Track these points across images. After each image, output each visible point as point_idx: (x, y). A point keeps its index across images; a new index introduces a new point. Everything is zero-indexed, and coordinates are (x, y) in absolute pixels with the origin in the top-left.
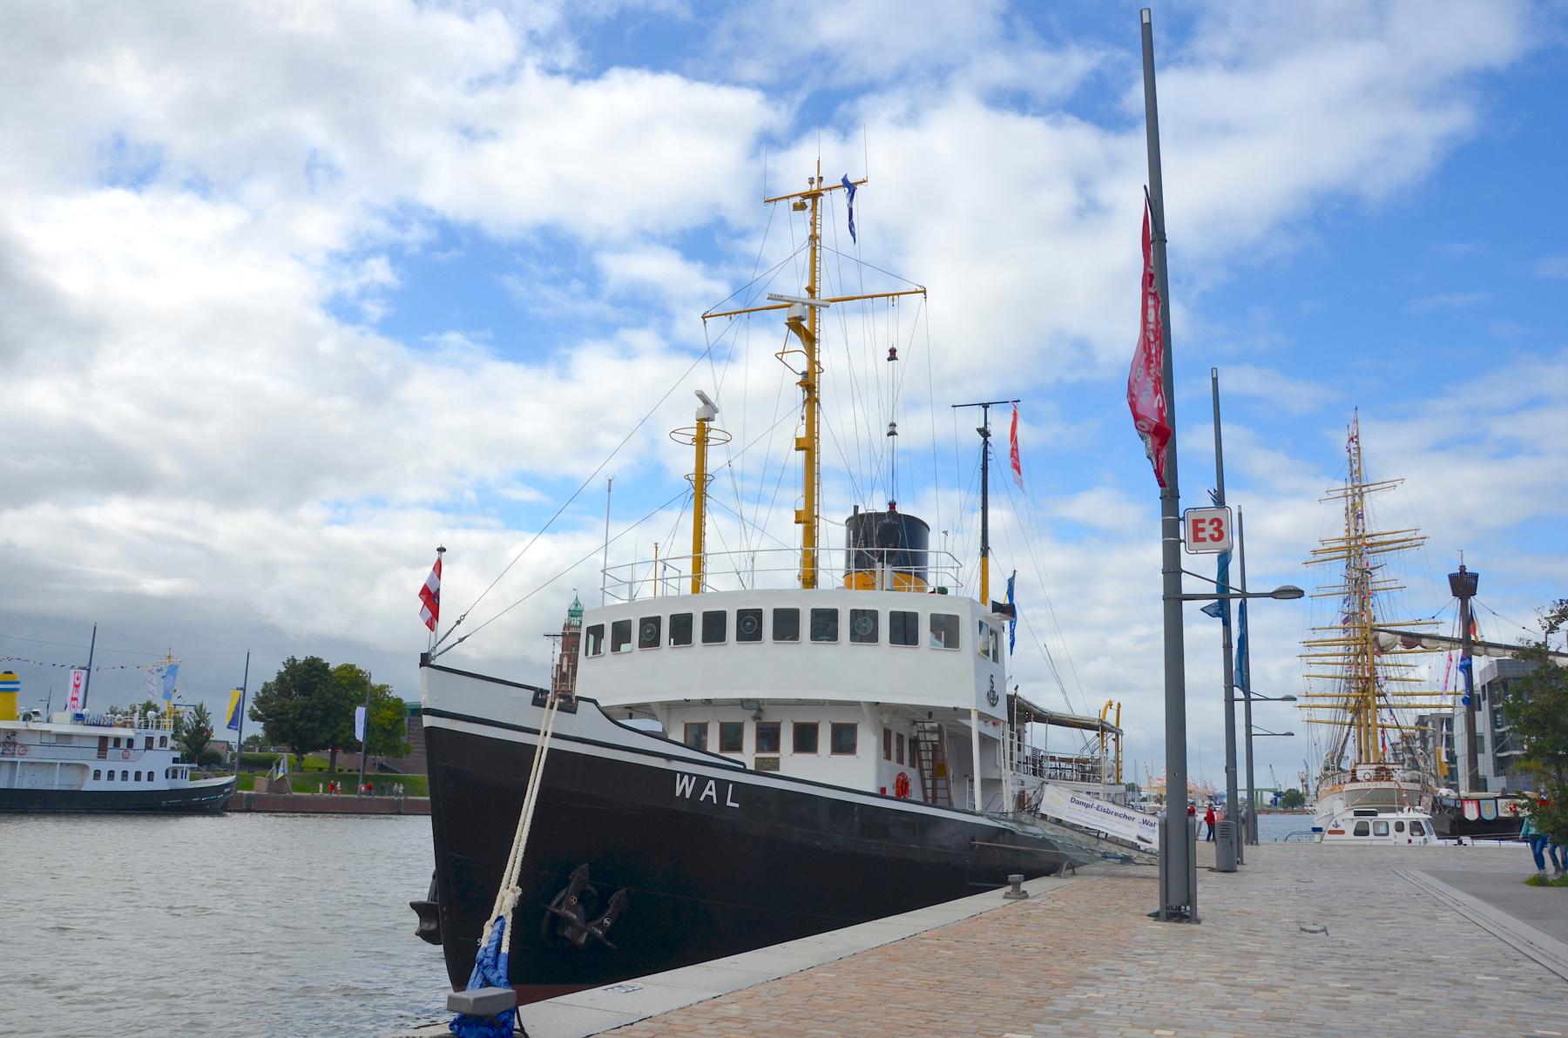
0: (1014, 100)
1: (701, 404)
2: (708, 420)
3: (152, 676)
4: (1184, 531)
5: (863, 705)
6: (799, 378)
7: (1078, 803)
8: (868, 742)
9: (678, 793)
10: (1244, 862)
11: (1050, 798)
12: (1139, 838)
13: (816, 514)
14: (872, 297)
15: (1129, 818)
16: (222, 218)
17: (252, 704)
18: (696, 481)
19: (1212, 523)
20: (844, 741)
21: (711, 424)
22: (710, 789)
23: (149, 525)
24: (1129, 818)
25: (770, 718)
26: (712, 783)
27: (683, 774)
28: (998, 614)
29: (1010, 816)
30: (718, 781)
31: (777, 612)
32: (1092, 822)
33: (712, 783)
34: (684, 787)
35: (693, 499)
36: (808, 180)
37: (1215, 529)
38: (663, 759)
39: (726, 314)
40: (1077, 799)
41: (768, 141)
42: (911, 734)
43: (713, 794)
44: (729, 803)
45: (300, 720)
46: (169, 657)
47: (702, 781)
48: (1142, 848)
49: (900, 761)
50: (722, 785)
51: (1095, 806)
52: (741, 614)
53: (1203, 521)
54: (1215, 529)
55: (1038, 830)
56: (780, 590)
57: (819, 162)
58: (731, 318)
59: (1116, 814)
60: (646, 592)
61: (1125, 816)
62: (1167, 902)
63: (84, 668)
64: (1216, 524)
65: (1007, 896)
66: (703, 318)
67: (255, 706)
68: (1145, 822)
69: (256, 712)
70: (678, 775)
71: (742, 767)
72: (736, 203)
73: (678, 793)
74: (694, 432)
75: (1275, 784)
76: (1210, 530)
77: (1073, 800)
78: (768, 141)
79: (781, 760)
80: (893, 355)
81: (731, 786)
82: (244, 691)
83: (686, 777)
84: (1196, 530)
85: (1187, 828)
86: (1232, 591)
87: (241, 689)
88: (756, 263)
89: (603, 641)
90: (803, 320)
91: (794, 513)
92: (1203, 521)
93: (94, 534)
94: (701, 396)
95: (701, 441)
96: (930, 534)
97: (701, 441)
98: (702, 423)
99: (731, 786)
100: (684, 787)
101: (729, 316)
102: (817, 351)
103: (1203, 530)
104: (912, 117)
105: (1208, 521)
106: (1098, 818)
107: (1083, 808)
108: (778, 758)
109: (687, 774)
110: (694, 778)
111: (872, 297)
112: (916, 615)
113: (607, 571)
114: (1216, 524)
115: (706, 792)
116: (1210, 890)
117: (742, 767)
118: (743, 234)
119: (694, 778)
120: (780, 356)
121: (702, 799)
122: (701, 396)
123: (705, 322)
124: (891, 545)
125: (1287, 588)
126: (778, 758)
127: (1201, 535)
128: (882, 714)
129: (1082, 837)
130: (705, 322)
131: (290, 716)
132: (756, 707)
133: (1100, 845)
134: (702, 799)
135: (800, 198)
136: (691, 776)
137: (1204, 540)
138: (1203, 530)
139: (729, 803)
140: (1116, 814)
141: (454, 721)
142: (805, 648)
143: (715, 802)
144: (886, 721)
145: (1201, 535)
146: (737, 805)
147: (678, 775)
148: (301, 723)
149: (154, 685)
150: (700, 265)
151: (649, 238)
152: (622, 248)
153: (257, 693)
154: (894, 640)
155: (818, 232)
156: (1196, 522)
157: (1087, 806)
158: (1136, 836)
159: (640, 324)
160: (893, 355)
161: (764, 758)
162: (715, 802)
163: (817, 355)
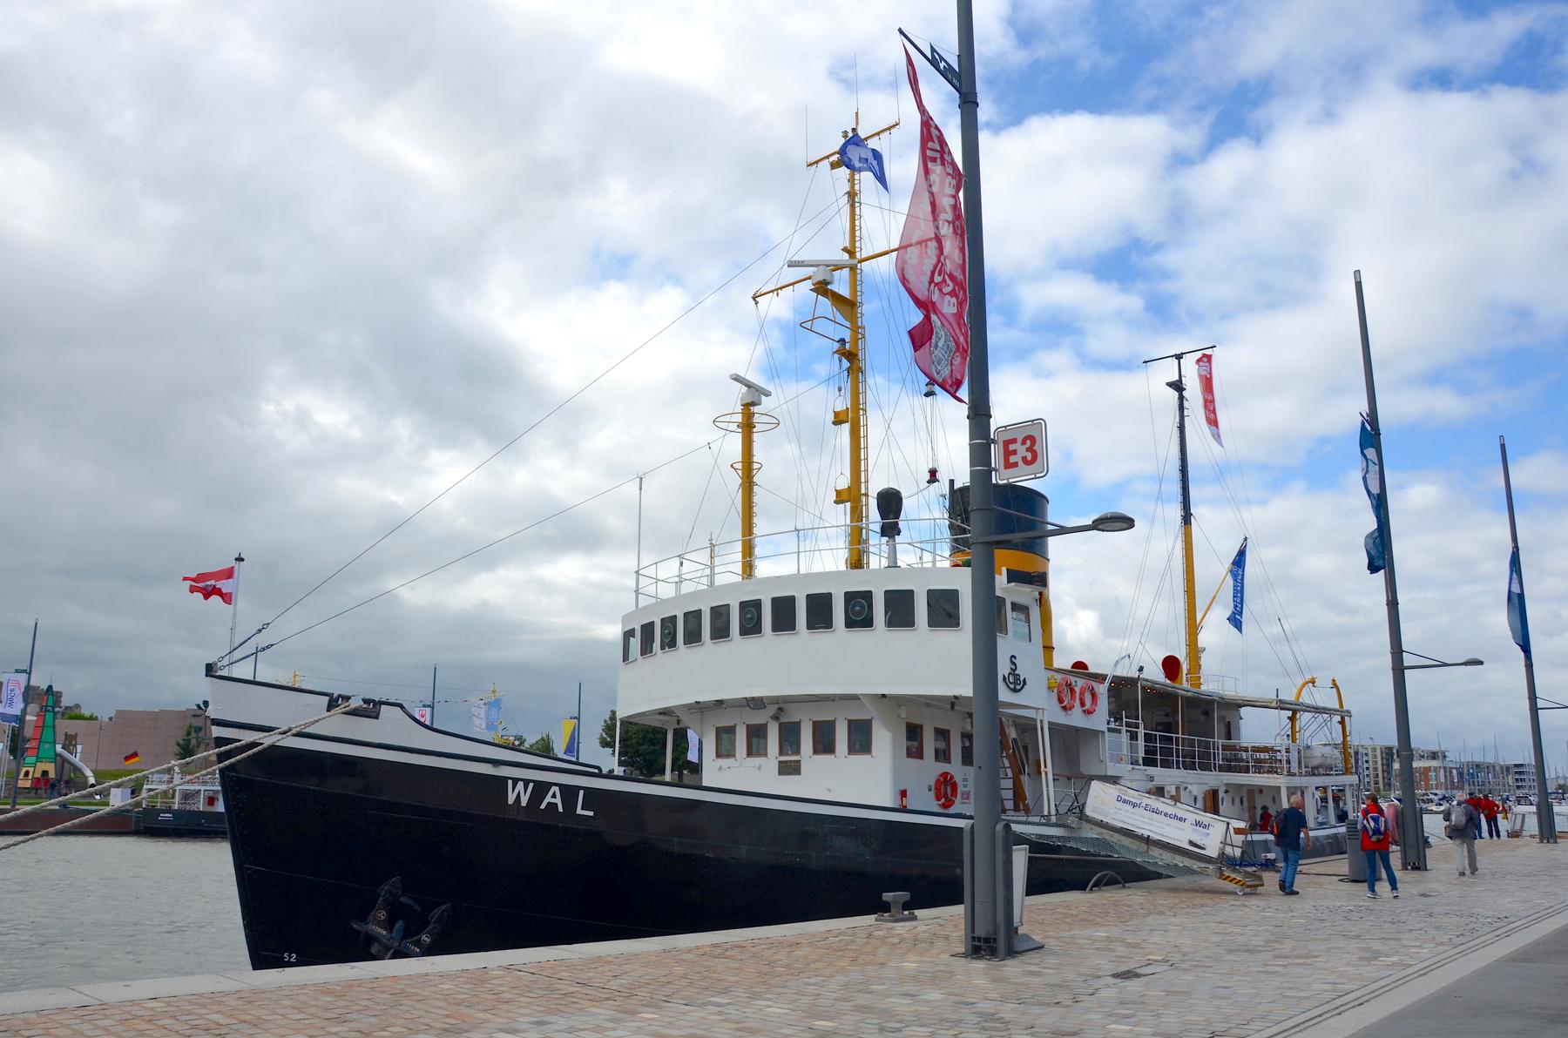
0: (1440, 79)
1: (745, 389)
2: (753, 404)
3: (479, 710)
4: (996, 452)
5: (863, 699)
6: (837, 346)
7: (1125, 801)
8: (884, 740)
10: (1428, 868)
11: (1095, 797)
12: (1192, 843)
13: (863, 491)
15: (1180, 819)
16: (671, 299)
17: (601, 731)
18: (743, 469)
19: (1024, 442)
20: (861, 741)
21: (755, 409)
22: (554, 796)
23: (595, 576)
24: (1180, 819)
25: (792, 716)
27: (516, 781)
28: (1013, 584)
29: (1053, 819)
30: (563, 787)
31: (775, 601)
32: (1138, 823)
34: (518, 795)
35: (741, 490)
36: (842, 134)
37: (1028, 450)
38: (490, 765)
39: (772, 291)
40: (1123, 797)
41: (1180, 161)
42: (964, 728)
43: (558, 801)
44: (579, 811)
45: (643, 744)
46: (494, 692)
47: (541, 788)
49: (943, 755)
50: (569, 793)
51: (1143, 805)
53: (1014, 441)
54: (1028, 450)
55: (1090, 833)
56: (778, 577)
57: (857, 113)
58: (778, 294)
59: (1166, 815)
60: (666, 591)
61: (1176, 817)
62: (973, 931)
63: (429, 706)
64: (1028, 443)
65: (876, 920)
66: (754, 298)
67: (604, 734)
68: (1198, 824)
69: (605, 739)
70: (510, 782)
71: (597, 771)
72: (1147, 221)
73: (511, 799)
74: (739, 418)
76: (1022, 451)
77: (1119, 799)
78: (1180, 161)
79: (802, 763)
81: (581, 792)
82: (579, 720)
83: (520, 785)
84: (1008, 453)
85: (994, 837)
86: (1050, 527)
87: (575, 718)
88: (1166, 275)
89: (654, 644)
90: (828, 283)
91: (835, 493)
92: (1014, 441)
93: (545, 587)
94: (737, 379)
95: (748, 427)
96: (1049, 506)
97: (748, 427)
98: (748, 407)
99: (581, 792)
100: (518, 795)
101: (776, 292)
102: (859, 315)
103: (1014, 452)
104: (1329, 116)
105: (1019, 441)
106: (1146, 820)
107: (1129, 807)
108: (799, 762)
109: (521, 780)
110: (531, 785)
112: (830, 595)
113: (641, 572)
114: (1028, 443)
115: (548, 799)
117: (597, 771)
118: (1158, 247)
119: (531, 785)
120: (808, 325)
121: (543, 807)
122: (737, 379)
123: (757, 303)
124: (891, 516)
125: (1104, 517)
126: (799, 762)
127: (1013, 459)
128: (899, 706)
129: (1131, 843)
130: (757, 303)
131: (634, 741)
132: (780, 705)
133: (1151, 853)
134: (543, 807)
135: (838, 156)
136: (526, 782)
137: (1015, 465)
138: (1014, 452)
139: (579, 811)
140: (1166, 815)
141: (241, 730)
142: (803, 637)
143: (561, 810)
144: (903, 715)
145: (1013, 459)
147: (510, 782)
148: (644, 747)
149: (482, 719)
150: (1115, 285)
151: (1070, 264)
152: (1040, 276)
153: (605, 721)
154: (933, 622)
155: (857, 187)
156: (1007, 443)
157: (1135, 805)
158: (1187, 841)
159: (1053, 345)
161: (787, 762)
162: (561, 810)
163: (859, 320)
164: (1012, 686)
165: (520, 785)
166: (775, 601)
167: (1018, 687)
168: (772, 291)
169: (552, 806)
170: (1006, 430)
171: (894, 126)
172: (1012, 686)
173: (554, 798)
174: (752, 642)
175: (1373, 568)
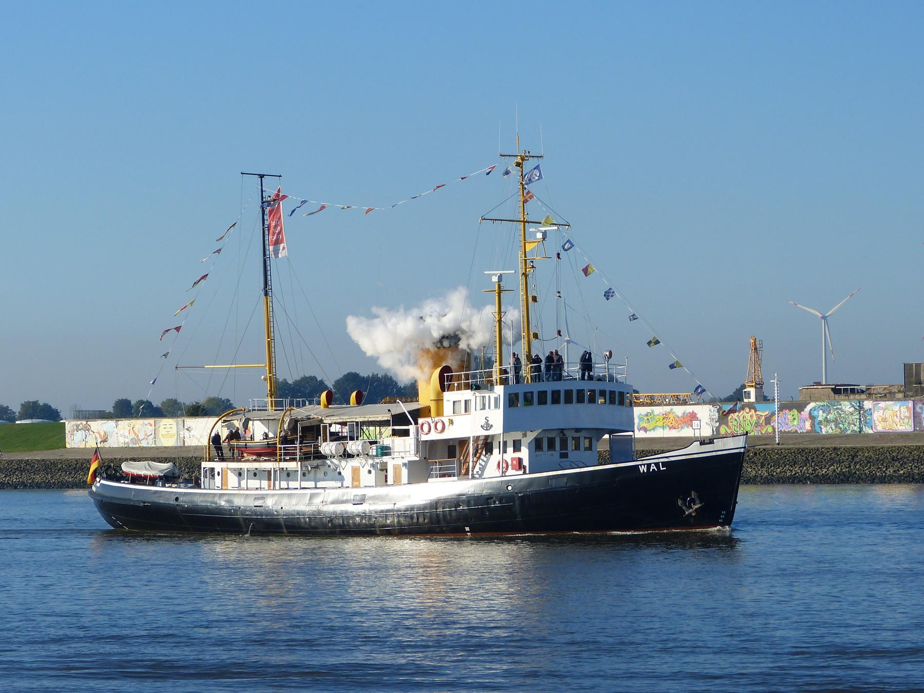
9: (642, 472)
14: (501, 220)
26: (653, 465)
27: (641, 465)
33: (653, 465)
34: (643, 469)
39: (491, 220)
43: (655, 468)
44: (662, 469)
48: (398, 648)
50: (657, 464)
52: (545, 403)
58: (265, 191)
70: (640, 466)
73: (642, 472)
75: (737, 523)
80: (608, 295)
81: (660, 464)
83: (643, 466)
99: (660, 464)
100: (643, 469)
110: (646, 466)
111: (501, 220)
115: (652, 468)
116: (768, 398)
119: (646, 466)
136: (644, 465)
139: (662, 469)
143: (656, 470)
146: (665, 468)
160: (608, 295)
162: (656, 470)
164: (485, 428)
165: (643, 466)
166: (578, 390)
167: (488, 428)
168: (491, 220)
169: (654, 470)
170: (260, 417)
171: (464, 178)
172: (485, 428)
173: (653, 467)
174: (556, 406)
175: (814, 383)
